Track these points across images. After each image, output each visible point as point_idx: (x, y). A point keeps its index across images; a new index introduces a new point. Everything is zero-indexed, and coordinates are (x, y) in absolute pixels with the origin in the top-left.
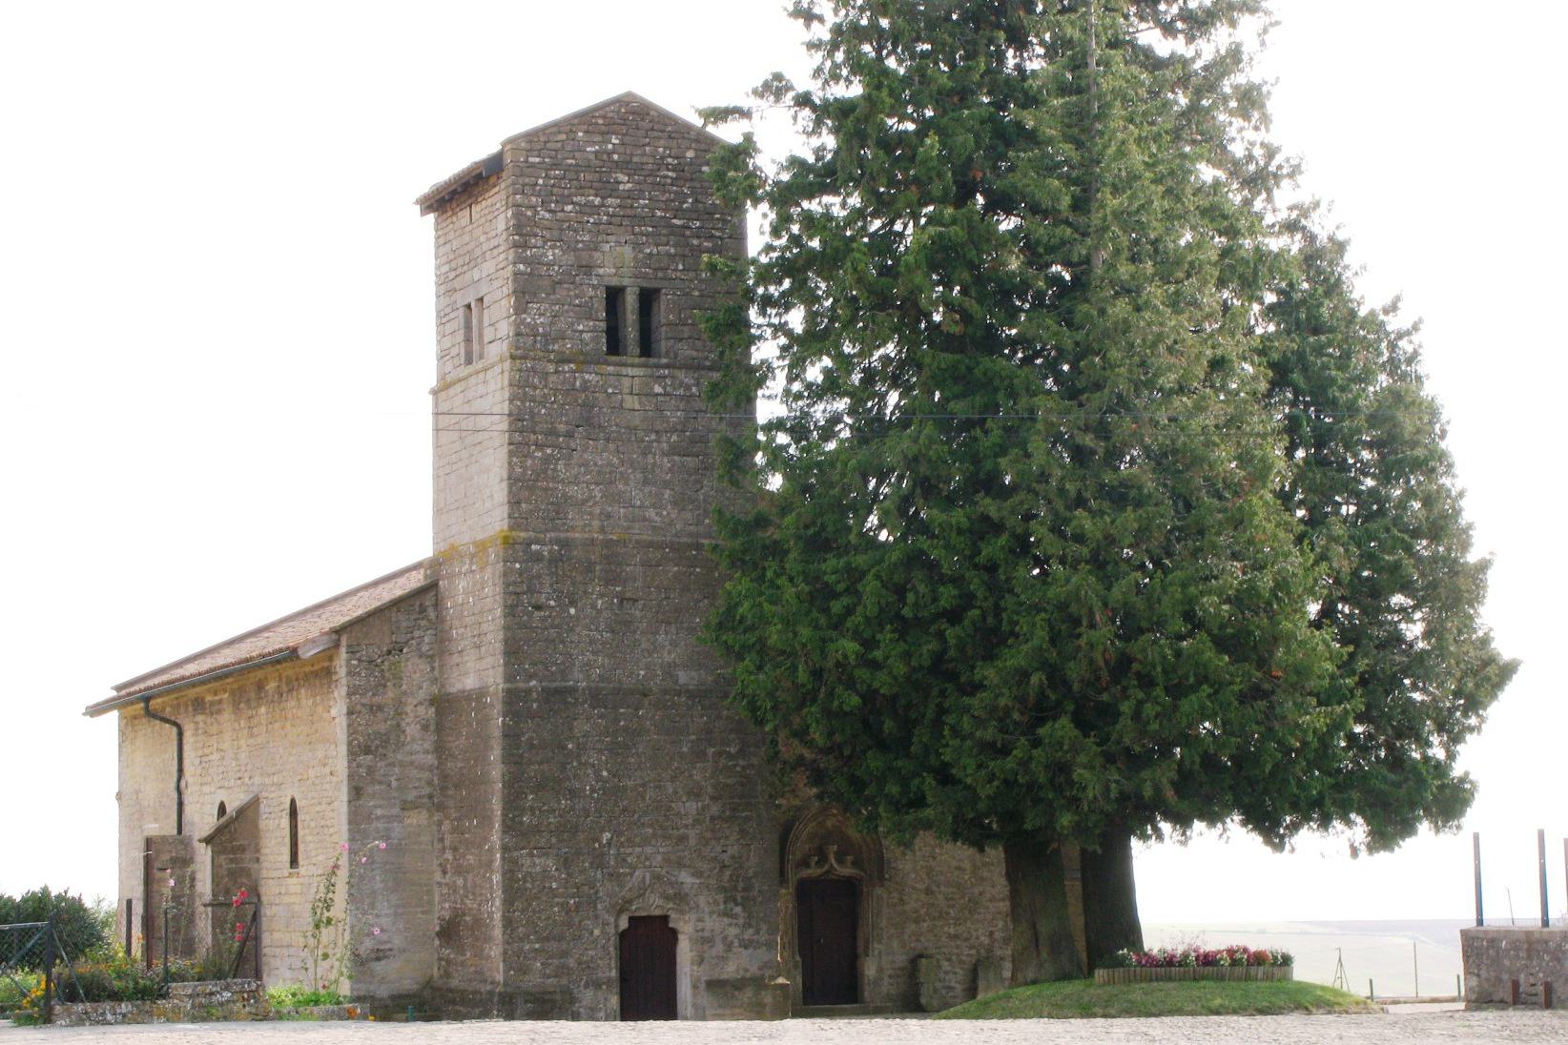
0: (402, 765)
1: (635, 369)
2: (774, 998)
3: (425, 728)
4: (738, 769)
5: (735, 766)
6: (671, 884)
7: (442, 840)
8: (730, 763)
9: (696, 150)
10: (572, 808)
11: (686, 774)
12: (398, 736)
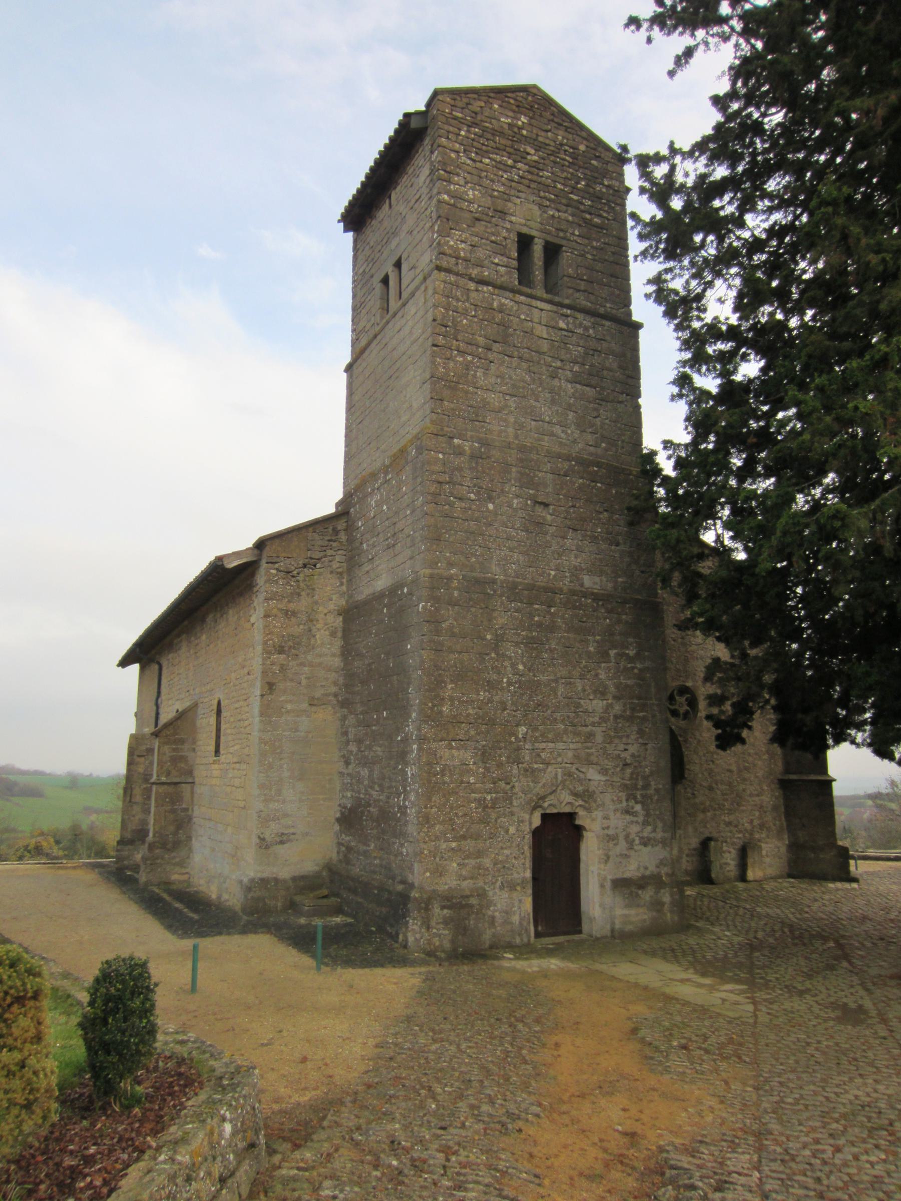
0: (311, 665)
1: (543, 303)
2: (672, 895)
3: (333, 634)
4: (636, 671)
5: (633, 668)
6: (580, 780)
7: (346, 733)
8: (629, 665)
9: (587, 147)
10: (490, 701)
11: (593, 673)
12: (309, 639)
